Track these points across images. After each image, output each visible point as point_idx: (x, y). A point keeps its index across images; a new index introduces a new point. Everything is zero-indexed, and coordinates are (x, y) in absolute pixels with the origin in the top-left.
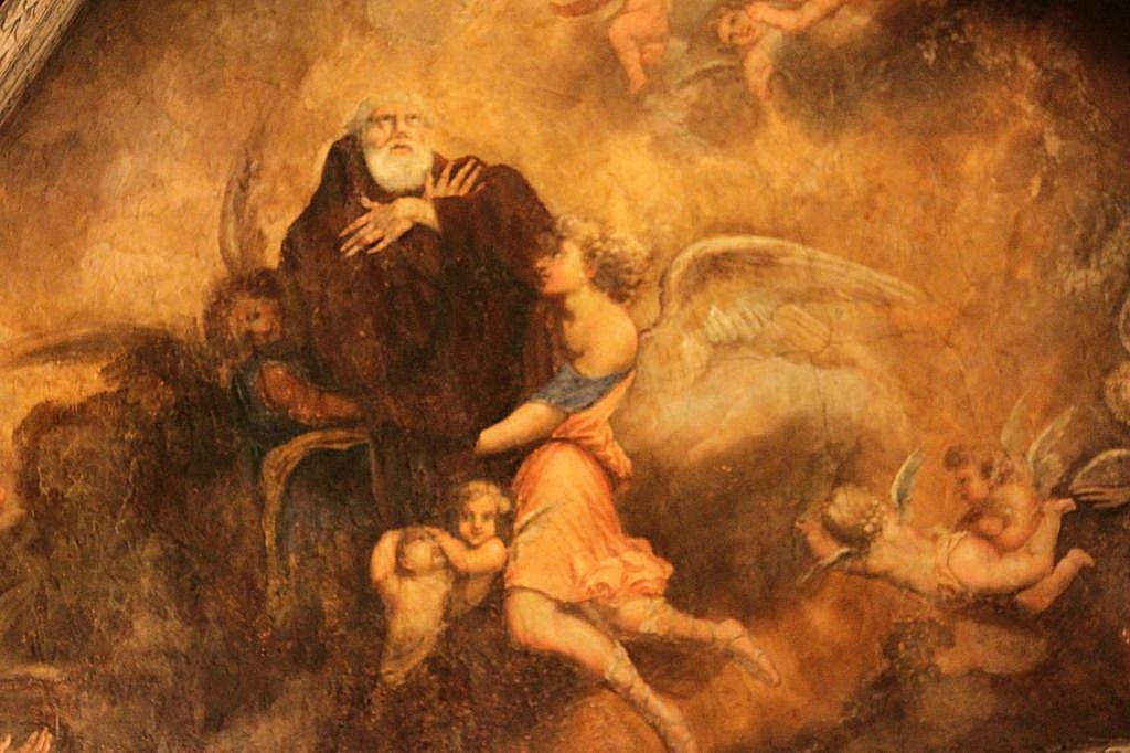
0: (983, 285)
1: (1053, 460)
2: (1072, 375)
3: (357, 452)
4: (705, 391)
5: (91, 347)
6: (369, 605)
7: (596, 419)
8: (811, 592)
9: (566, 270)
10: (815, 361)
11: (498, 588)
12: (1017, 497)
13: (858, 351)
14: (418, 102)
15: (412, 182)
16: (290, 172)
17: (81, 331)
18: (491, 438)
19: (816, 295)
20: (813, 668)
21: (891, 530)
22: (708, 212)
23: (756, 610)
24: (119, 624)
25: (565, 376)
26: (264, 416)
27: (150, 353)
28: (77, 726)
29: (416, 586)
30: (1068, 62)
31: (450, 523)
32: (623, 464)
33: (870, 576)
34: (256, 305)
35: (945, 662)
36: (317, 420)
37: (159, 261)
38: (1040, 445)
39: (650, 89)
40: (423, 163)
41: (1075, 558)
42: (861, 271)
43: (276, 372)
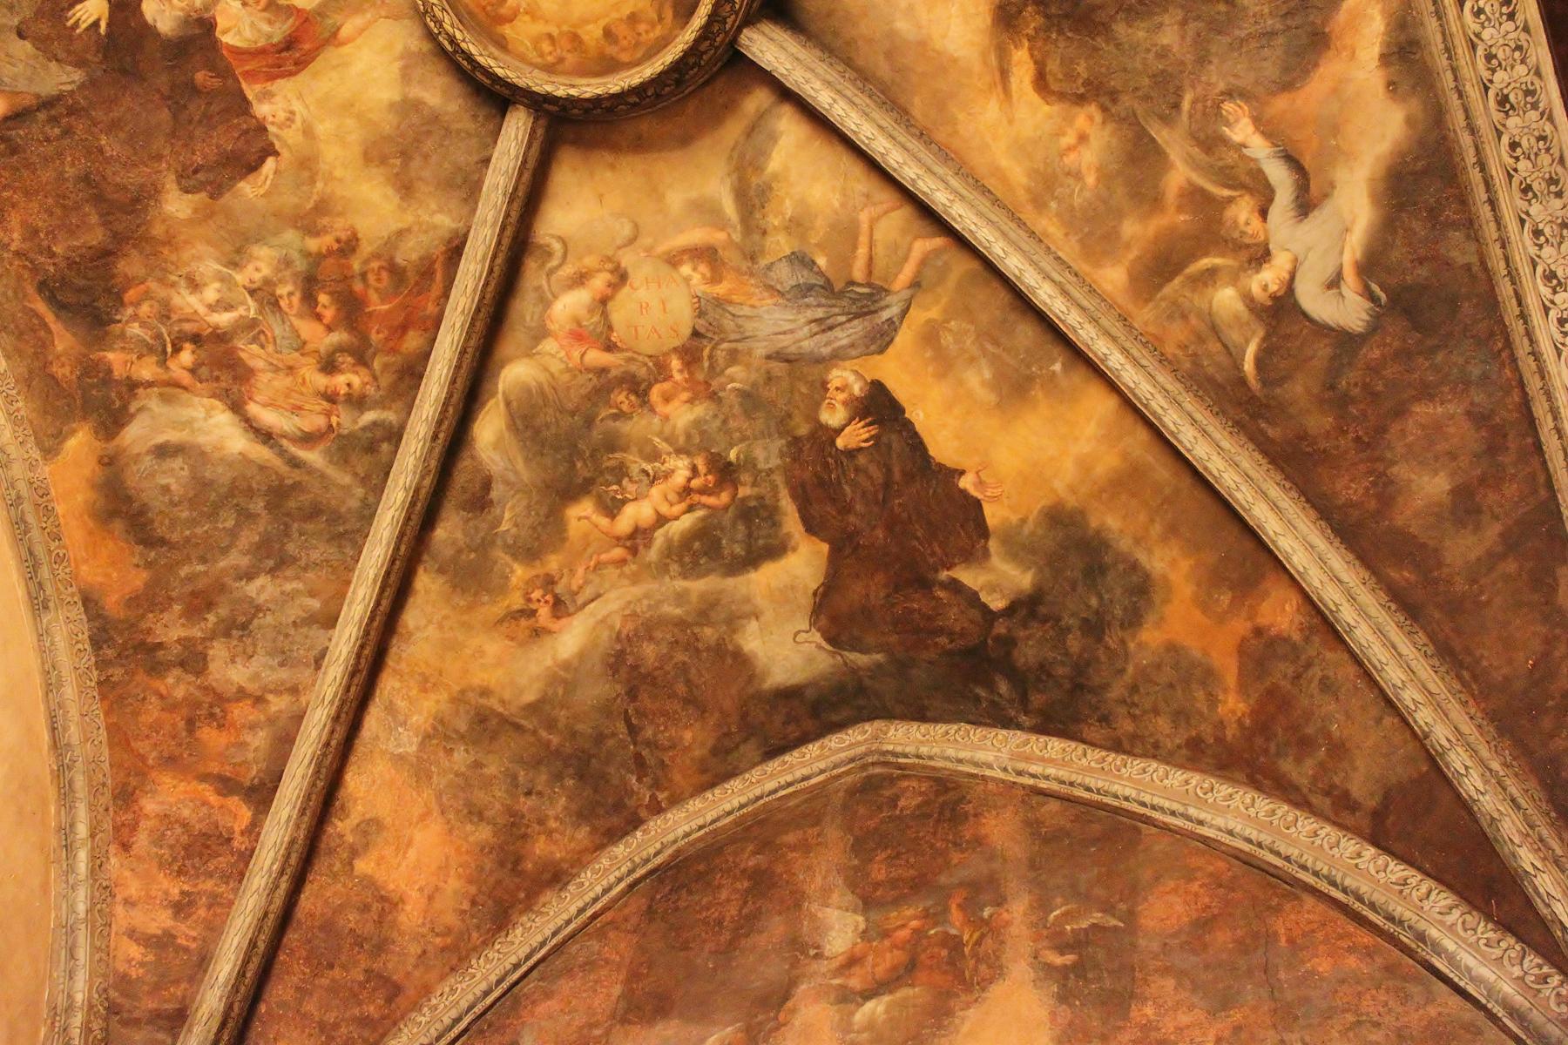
24: (1164, 53)
28: (1222, 86)
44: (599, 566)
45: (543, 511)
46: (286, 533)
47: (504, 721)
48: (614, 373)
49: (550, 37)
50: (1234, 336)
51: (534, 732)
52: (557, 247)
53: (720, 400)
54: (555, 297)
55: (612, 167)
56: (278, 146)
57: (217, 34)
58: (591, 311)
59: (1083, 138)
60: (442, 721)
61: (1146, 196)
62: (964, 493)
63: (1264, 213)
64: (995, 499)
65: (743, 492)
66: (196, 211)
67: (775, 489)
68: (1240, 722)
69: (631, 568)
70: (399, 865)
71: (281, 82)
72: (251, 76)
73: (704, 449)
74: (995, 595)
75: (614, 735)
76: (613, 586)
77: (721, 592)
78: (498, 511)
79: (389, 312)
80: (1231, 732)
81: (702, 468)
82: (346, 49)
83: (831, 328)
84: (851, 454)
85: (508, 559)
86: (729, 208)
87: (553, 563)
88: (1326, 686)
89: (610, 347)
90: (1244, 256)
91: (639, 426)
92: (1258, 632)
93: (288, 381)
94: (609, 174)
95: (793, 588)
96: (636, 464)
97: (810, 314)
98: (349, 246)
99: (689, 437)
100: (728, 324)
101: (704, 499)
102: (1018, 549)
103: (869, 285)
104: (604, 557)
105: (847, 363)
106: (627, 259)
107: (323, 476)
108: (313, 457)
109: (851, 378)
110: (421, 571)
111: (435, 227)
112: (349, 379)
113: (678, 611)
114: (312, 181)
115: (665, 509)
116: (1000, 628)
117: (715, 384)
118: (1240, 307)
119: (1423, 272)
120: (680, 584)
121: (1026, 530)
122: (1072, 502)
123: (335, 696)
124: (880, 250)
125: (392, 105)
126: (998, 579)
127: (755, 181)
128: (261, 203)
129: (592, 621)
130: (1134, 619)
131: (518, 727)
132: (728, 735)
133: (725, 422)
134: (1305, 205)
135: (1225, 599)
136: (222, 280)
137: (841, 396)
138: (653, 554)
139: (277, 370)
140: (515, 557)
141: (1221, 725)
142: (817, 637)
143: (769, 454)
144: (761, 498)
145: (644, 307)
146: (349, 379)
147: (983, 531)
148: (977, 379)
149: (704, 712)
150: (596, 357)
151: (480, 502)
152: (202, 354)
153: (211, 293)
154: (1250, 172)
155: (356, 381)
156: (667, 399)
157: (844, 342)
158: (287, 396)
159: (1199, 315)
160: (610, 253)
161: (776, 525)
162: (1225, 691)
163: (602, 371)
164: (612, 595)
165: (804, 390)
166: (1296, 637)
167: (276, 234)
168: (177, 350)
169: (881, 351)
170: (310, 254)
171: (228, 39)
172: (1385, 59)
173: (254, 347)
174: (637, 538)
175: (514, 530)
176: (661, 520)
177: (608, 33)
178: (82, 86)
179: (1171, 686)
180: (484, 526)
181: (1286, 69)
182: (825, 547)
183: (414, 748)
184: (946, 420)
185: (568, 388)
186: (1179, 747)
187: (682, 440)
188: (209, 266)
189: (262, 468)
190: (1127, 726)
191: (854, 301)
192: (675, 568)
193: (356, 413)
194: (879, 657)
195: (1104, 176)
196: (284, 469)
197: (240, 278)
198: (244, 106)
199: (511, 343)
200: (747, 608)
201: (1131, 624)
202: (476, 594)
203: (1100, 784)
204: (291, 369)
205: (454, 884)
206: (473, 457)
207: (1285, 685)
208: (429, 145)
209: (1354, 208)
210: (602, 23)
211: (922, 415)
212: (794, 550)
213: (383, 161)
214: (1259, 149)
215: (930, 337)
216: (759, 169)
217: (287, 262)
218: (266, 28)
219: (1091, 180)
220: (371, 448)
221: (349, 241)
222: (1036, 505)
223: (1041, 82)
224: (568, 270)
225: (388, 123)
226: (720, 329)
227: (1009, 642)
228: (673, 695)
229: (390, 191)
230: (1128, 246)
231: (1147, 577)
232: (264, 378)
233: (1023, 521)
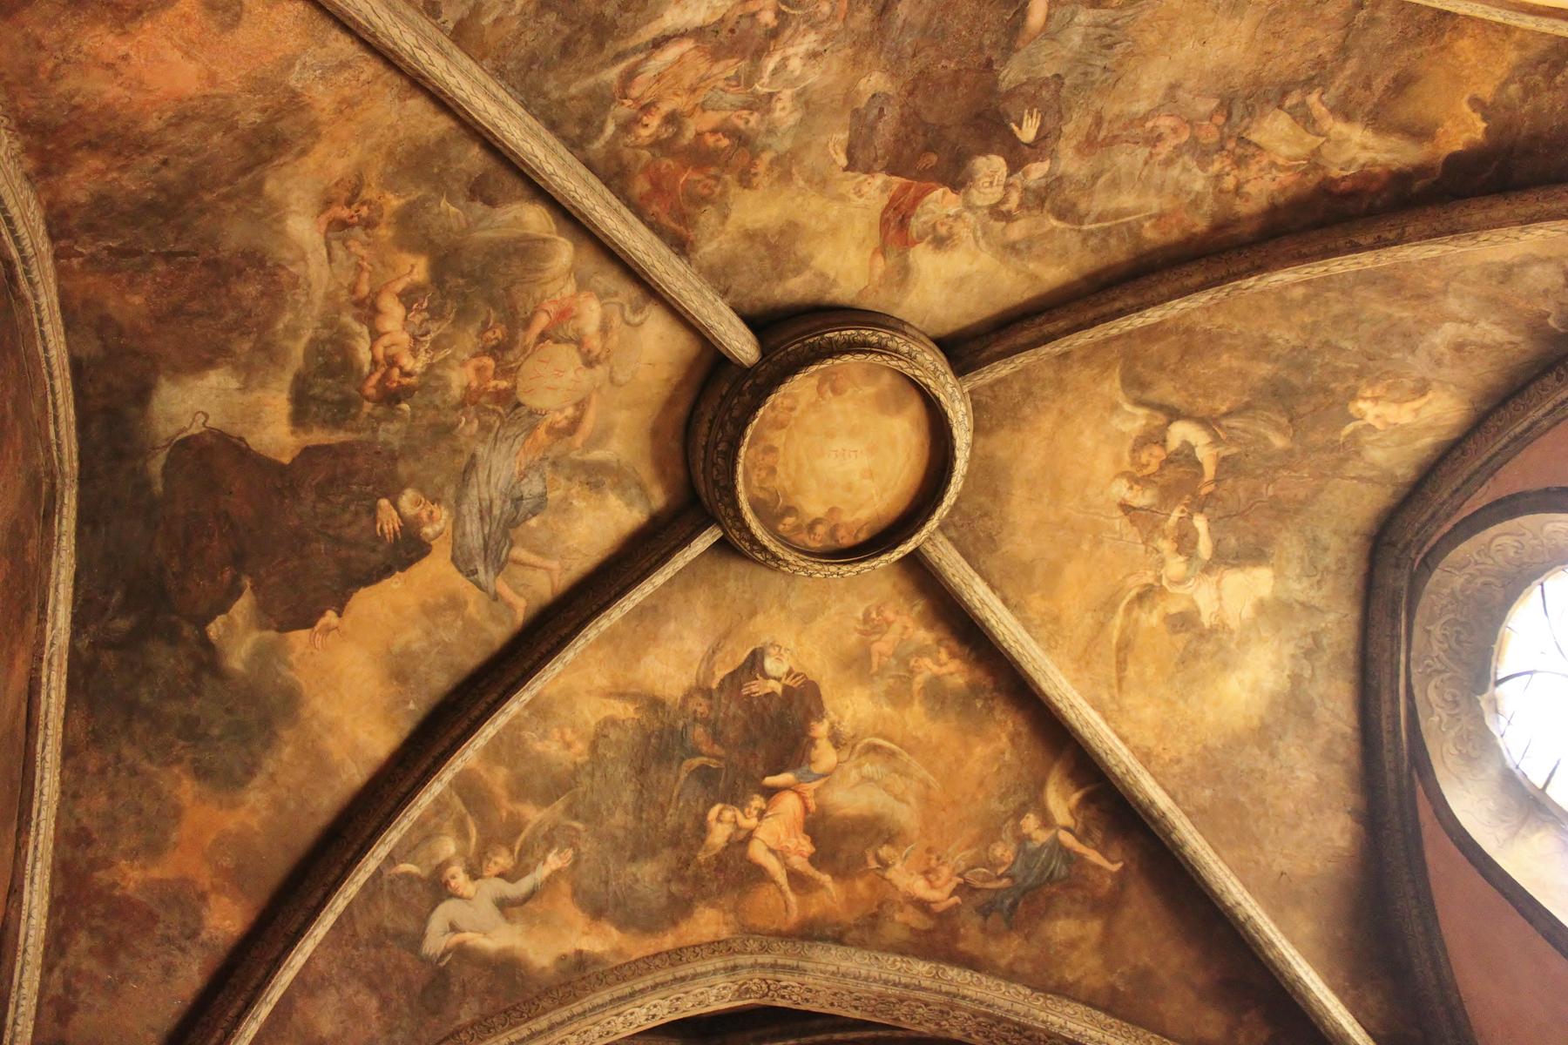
0: (964, 795)
1: (963, 864)
2: (981, 838)
3: (718, 770)
4: (852, 795)
5: (634, 697)
6: (702, 828)
7: (809, 788)
8: (861, 876)
9: (821, 730)
10: (895, 797)
11: (750, 835)
12: (945, 871)
13: (912, 799)
14: (792, 645)
15: (777, 675)
16: (734, 653)
17: (633, 690)
18: (770, 781)
19: (905, 774)
20: (850, 902)
21: (898, 866)
22: (879, 728)
23: (840, 875)
24: (611, 813)
25: (805, 768)
26: (689, 744)
27: (655, 704)
28: (583, 849)
29: (721, 827)
30: (1024, 729)
31: (742, 807)
32: (813, 808)
33: (884, 878)
34: (701, 700)
35: (898, 917)
36: (710, 754)
37: (671, 671)
38: (959, 856)
39: (877, 674)
40: (785, 669)
41: (956, 899)
42: (924, 772)
43: (699, 730)
44: (359, 268)
45: (438, 240)
46: (565, 20)
47: (264, 161)
48: (521, 334)
49: (792, 409)
50: (422, 854)
51: (229, 183)
52: (637, 319)
53: (456, 408)
54: (602, 306)
55: (669, 380)
56: (850, 174)
57: (947, 189)
58: (578, 331)
59: (568, 746)
60: (302, 109)
61: (521, 790)
62: (322, 613)
63: (501, 875)
64: (312, 643)
65: (368, 407)
66: (858, 93)
67: (358, 431)
68: (114, 885)
69: (344, 296)
70: (170, 39)
71: (886, 202)
72: (905, 189)
73: (421, 388)
74: (222, 630)
75: (177, 240)
76: (334, 276)
77: (283, 367)
78: (462, 203)
79: (677, 180)
80: (102, 876)
81: (406, 381)
82: (869, 254)
83: (482, 518)
84: (373, 511)
85: (413, 197)
86: (597, 455)
87: (385, 233)
88: (168, 970)
89: (543, 337)
90: (474, 861)
91: (469, 339)
92: (203, 897)
93: (686, 83)
94: (665, 375)
95: (256, 423)
96: (436, 329)
97: (498, 503)
98: (746, 180)
99: (439, 378)
100: (512, 431)
101: (377, 376)
102: (263, 655)
103: (507, 560)
104: (366, 276)
105: (449, 528)
106: (600, 371)
107: (591, 72)
108: (612, 74)
109: (437, 528)
110: (453, 124)
111: (710, 240)
112: (653, 125)
113: (280, 326)
114: (808, 181)
115: (385, 340)
116: (188, 631)
117: (472, 409)
118: (442, 858)
119: (456, 989)
120: (307, 335)
121: (282, 669)
122: (305, 713)
123: (417, 61)
124: (529, 573)
125: (812, 257)
126: (238, 635)
127: (608, 481)
128: (823, 139)
129: (309, 249)
130: (202, 773)
131: (246, 170)
132: (120, 334)
133: (436, 408)
134: (504, 906)
135: (227, 862)
136: (797, 79)
137: (424, 515)
138: (347, 319)
139: (702, 79)
140: (411, 204)
141: (108, 864)
142: (195, 431)
143: (390, 433)
144: (355, 417)
145: (559, 373)
146: (653, 125)
147: (285, 627)
148: (413, 637)
149: (158, 320)
150: (542, 321)
151: (480, 191)
152: (759, 32)
153: (795, 65)
154: (528, 866)
155: (644, 133)
156: (479, 370)
157: (468, 528)
158: (676, 76)
159: (438, 826)
160: (612, 360)
161: (324, 424)
162: (144, 867)
163: (527, 324)
164: (325, 273)
165: (438, 480)
166: (204, 936)
167: (796, 137)
168: (779, 13)
169: (454, 559)
170: (763, 150)
171: (939, 192)
172: (579, 953)
173: (732, 73)
174: (369, 310)
175: (436, 210)
176: (376, 335)
177: (772, 450)
178: (996, 83)
179: (140, 811)
180: (456, 187)
181: (584, 892)
182: (286, 460)
183: (292, 83)
184: (388, 606)
185: (528, 294)
186: (78, 821)
187: (438, 372)
188: (815, 77)
189: (635, 28)
190: (93, 764)
191: (498, 543)
192: (325, 334)
193: (621, 121)
194: (159, 488)
195: (539, 757)
196: (622, 46)
197: (787, 93)
198: (892, 170)
199: (590, 262)
200: (254, 383)
201: (196, 770)
202: (400, 163)
203: (48, 758)
204: (693, 90)
205: (112, 91)
206: (519, 198)
207: (159, 930)
208: (768, 264)
209: (496, 938)
210: (781, 449)
211: (395, 586)
212: (293, 433)
213: (782, 233)
214: (542, 873)
215: (455, 603)
216: (615, 486)
217: (771, 132)
218: (923, 219)
219: (539, 747)
220: (585, 121)
221: (749, 181)
222: (302, 678)
223: (612, 722)
224: (616, 321)
225: (802, 249)
226: (511, 424)
227: (173, 637)
228: (192, 296)
229: (758, 225)
230: (488, 770)
231: (240, 784)
232: (703, 67)
233: (291, 667)
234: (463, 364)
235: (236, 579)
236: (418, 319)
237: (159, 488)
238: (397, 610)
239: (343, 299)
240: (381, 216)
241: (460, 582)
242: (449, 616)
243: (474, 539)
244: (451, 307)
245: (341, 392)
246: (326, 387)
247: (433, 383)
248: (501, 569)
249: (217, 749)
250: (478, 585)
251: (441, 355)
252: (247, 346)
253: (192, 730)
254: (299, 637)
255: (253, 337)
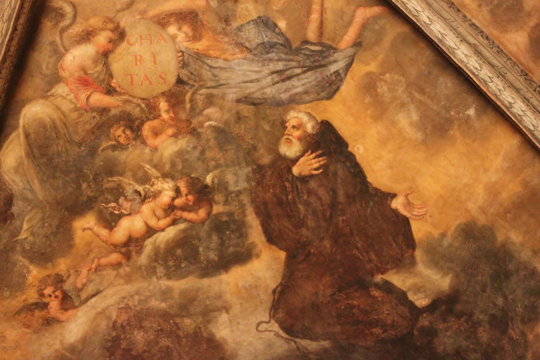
44: (98, 269)
48: (113, 112)
58: (95, 62)
62: (395, 212)
64: (421, 217)
65: (217, 209)
67: (242, 206)
78: (18, 223)
81: (184, 189)
83: (289, 78)
84: (304, 179)
85: (26, 262)
87: (62, 265)
89: (110, 91)
95: (256, 287)
96: (131, 186)
97: (273, 67)
99: (173, 164)
100: (206, 74)
101: (187, 215)
102: (438, 257)
103: (320, 44)
104: (103, 261)
105: (302, 107)
106: (125, 21)
113: (163, 305)
115: (153, 222)
116: (424, 321)
120: (165, 283)
121: (446, 243)
124: (329, 16)
126: (422, 281)
129: (93, 313)
133: (203, 152)
137: (297, 133)
138: (143, 259)
140: (31, 260)
142: (276, 327)
143: (238, 179)
147: (410, 243)
148: (406, 121)
150: (99, 99)
156: (156, 134)
157: (300, 90)
160: (111, 15)
163: (104, 110)
164: (109, 292)
169: (330, 97)
174: (131, 245)
175: (31, 239)
176: (150, 231)
182: (283, 255)
187: (167, 167)
192: (161, 270)
194: (326, 344)
199: (33, 84)
201: (530, 320)
212: (258, 256)
215: (369, 86)
222: (454, 223)
224: (77, 29)
226: (200, 78)
227: (431, 333)
234: (155, 149)
235: (377, 286)
236: (126, 205)
237: (326, 344)
238: (383, 142)
239: (127, 269)
240: (49, 276)
241: (348, 87)
242: (383, 89)
243: (310, 79)
244: (110, 183)
245: (209, 236)
246: (207, 248)
247: (180, 167)
248: (330, 47)
249: (514, 300)
250: (349, 66)
251: (153, 172)
252: (187, 321)
253: (500, 322)
254: (418, 230)
255: (178, 320)
